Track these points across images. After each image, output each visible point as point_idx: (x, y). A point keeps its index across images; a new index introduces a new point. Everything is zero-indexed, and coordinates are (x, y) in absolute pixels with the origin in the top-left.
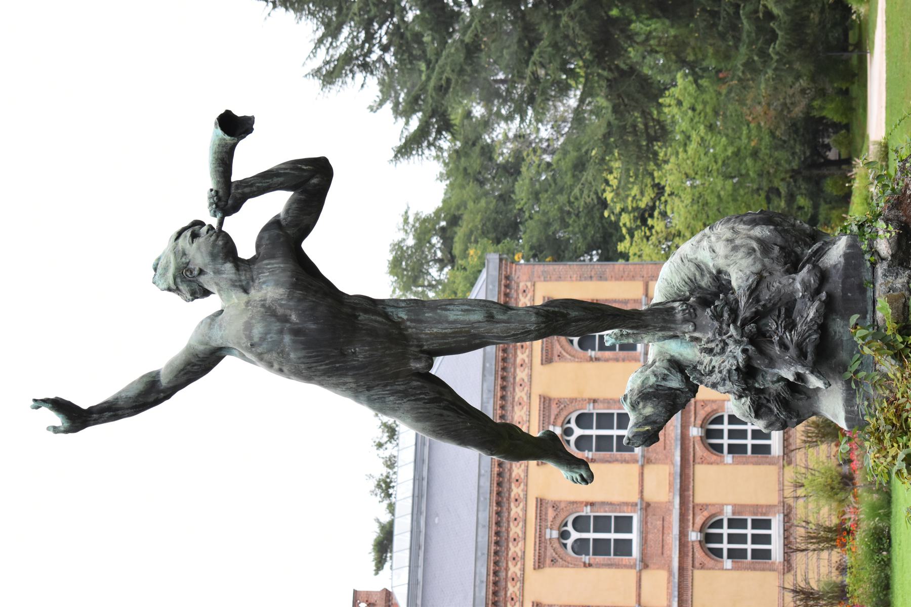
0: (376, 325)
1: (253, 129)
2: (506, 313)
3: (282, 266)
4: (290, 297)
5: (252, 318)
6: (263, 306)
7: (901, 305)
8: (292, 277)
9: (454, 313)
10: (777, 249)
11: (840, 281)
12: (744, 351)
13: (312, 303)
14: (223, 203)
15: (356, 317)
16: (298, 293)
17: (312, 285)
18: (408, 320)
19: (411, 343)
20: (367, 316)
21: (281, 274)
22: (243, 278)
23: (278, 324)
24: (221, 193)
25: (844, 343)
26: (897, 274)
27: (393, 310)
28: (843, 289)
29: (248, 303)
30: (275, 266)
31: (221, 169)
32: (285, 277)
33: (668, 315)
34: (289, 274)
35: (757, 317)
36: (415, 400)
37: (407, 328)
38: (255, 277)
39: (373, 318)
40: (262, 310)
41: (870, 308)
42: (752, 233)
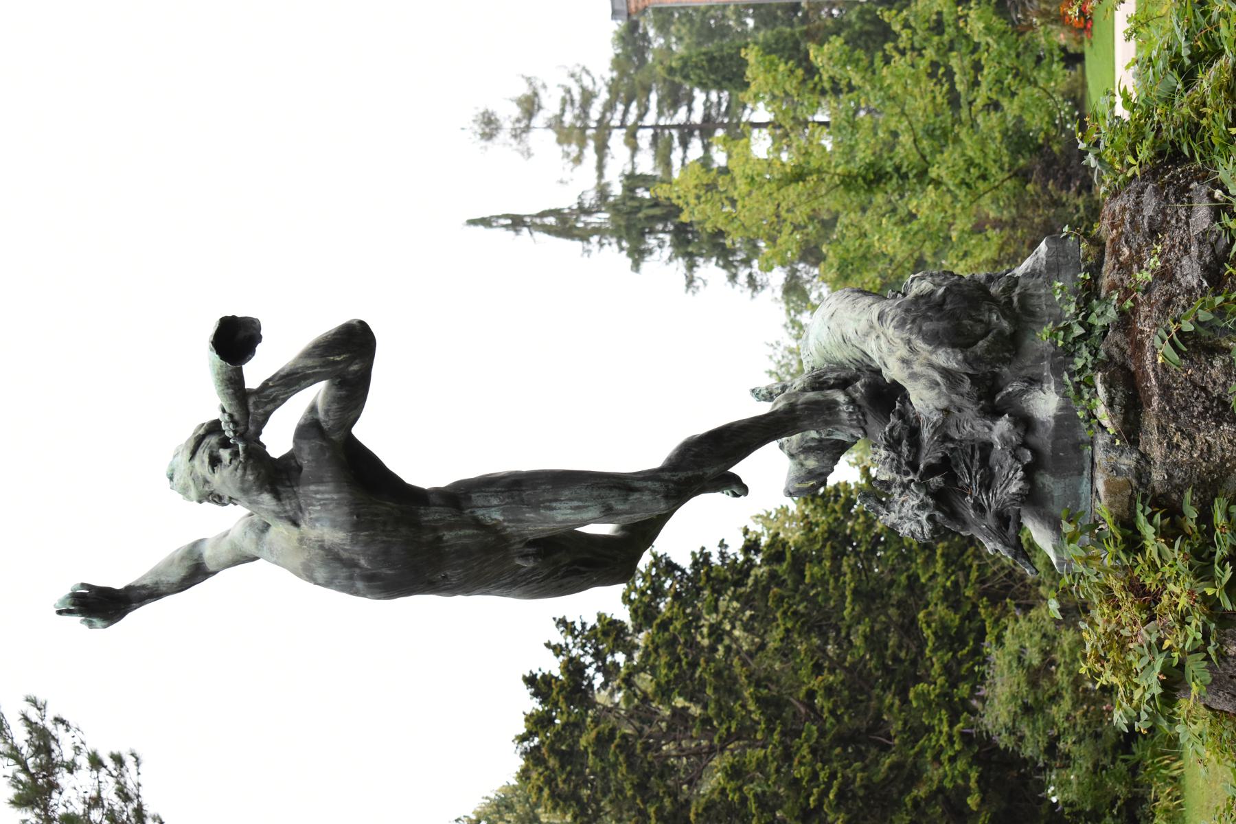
0: (466, 541)
1: (261, 337)
2: (627, 500)
3: (335, 496)
4: (354, 541)
5: (310, 560)
6: (322, 547)
7: (1126, 500)
8: (351, 514)
9: (562, 512)
10: (968, 381)
11: (1050, 441)
12: (931, 518)
13: (382, 545)
14: (242, 427)
15: (440, 539)
16: (363, 535)
17: (377, 515)
18: (504, 521)
19: (512, 542)
20: (453, 534)
21: (336, 511)
22: (288, 508)
23: (344, 570)
24: (237, 417)
25: (1056, 499)
26: (1122, 451)
27: (485, 512)
28: (1054, 449)
29: (301, 540)
30: (327, 496)
31: (230, 391)
32: (342, 514)
33: (831, 415)
34: (346, 509)
35: (944, 466)
36: (527, 584)
37: (504, 528)
38: (303, 506)
39: (461, 533)
40: (322, 552)
41: (1088, 465)
42: (934, 358)
